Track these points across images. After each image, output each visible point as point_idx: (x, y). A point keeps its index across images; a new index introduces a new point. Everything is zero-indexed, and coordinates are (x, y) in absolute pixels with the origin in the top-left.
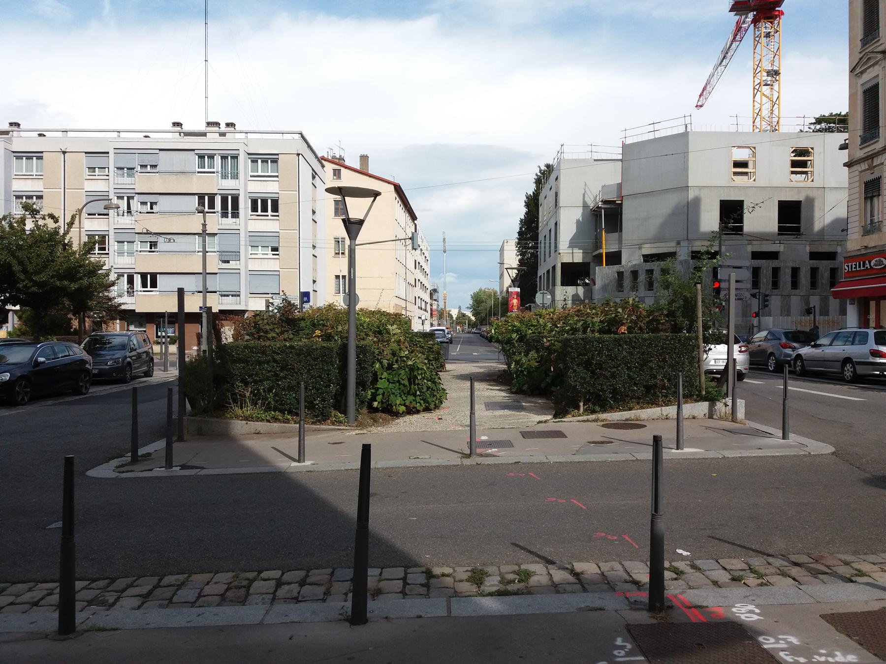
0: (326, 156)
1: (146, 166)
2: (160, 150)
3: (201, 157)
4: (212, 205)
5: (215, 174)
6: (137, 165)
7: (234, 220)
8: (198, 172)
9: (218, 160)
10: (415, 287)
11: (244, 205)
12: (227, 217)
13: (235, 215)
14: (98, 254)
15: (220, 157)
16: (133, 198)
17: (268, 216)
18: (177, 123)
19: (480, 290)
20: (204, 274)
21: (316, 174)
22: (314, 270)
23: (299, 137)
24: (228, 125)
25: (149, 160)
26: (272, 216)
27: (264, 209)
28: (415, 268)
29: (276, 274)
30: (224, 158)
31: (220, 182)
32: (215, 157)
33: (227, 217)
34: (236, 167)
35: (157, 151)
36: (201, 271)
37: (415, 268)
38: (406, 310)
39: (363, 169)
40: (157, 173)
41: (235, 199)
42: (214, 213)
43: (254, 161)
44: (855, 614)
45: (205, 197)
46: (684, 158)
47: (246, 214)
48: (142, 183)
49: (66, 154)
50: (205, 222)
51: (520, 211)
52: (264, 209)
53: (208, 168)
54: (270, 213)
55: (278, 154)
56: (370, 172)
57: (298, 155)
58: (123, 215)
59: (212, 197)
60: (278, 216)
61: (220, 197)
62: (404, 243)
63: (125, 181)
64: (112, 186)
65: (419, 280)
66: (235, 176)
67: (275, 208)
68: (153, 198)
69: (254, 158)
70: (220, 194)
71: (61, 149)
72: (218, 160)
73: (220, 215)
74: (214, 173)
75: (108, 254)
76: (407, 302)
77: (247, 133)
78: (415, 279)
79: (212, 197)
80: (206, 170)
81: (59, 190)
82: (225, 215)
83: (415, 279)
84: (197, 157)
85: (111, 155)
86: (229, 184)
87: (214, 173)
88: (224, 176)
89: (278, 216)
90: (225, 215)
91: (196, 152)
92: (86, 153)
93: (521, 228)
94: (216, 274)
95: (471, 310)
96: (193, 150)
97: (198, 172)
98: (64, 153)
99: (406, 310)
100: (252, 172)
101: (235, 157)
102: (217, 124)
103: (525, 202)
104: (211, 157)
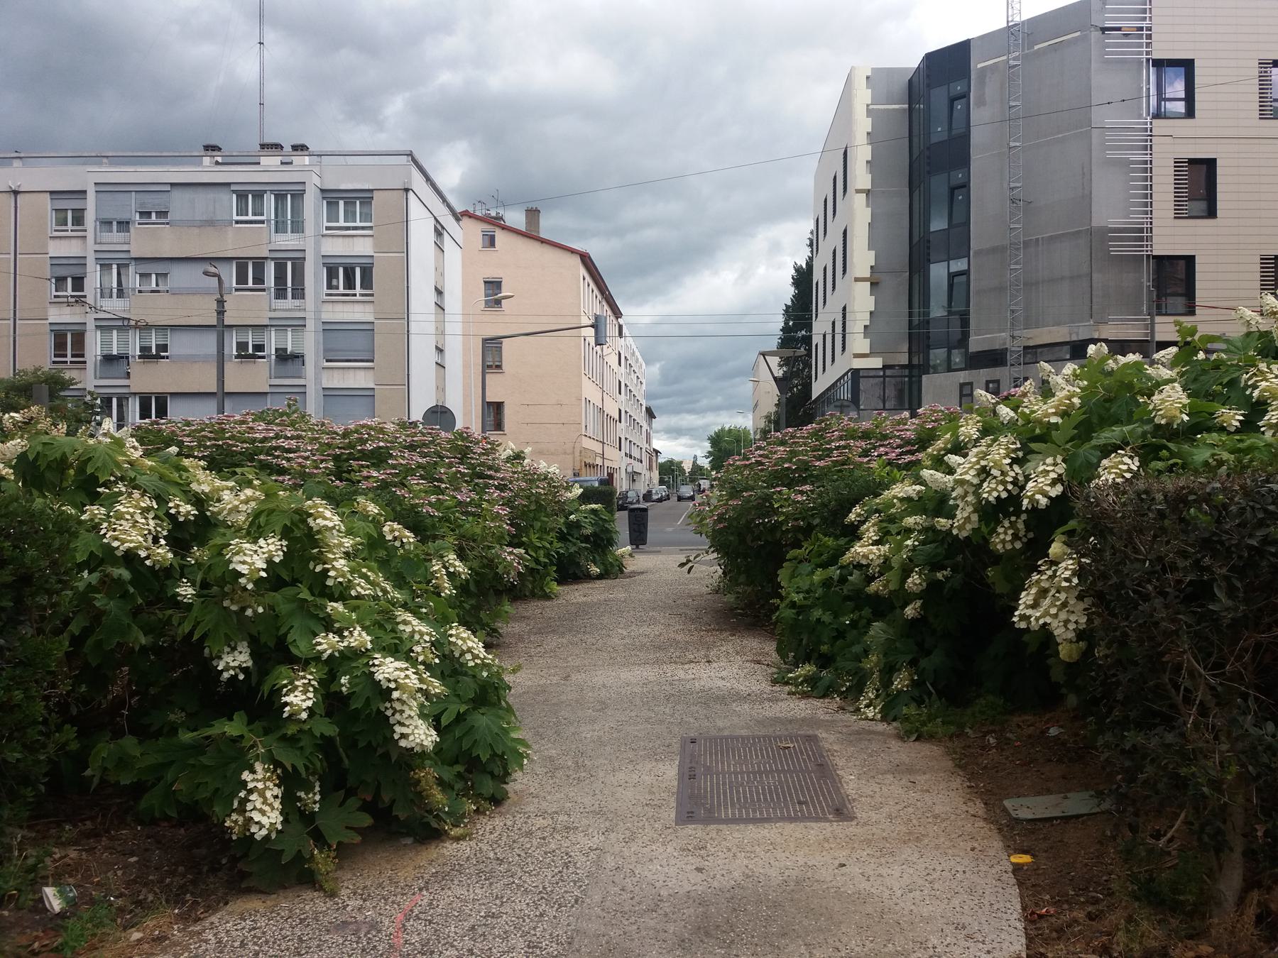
0: (471, 210)
1: (149, 214)
2: (172, 184)
3: (242, 196)
4: (259, 279)
5: (265, 225)
6: (133, 212)
7: (297, 302)
8: (237, 222)
9: (270, 202)
10: (620, 422)
11: (314, 277)
12: (285, 298)
13: (299, 293)
14: (71, 362)
15: (273, 196)
16: (127, 266)
17: (355, 295)
18: (212, 147)
19: (723, 429)
20: (220, 395)
21: (443, 228)
22: (440, 389)
23: (408, 161)
24: (296, 148)
25: (152, 203)
26: (362, 295)
27: (350, 284)
28: (620, 393)
29: (367, 395)
30: (280, 197)
31: (273, 239)
32: (265, 195)
33: (285, 298)
34: (297, 211)
35: (168, 188)
36: (214, 390)
37: (620, 393)
38: (603, 458)
39: (531, 231)
40: (168, 224)
41: (299, 265)
42: (264, 290)
43: (332, 204)
44: (463, 296)
45: (247, 263)
46: (1083, 178)
47: (317, 293)
48: (142, 241)
49: (18, 196)
50: (222, 296)
51: (787, 292)
52: (350, 284)
53: (254, 214)
54: (358, 290)
55: (372, 191)
56: (542, 235)
57: (407, 190)
58: (111, 297)
59: (259, 264)
60: (372, 295)
61: (273, 264)
62: (599, 352)
63: (114, 238)
64: (91, 245)
65: (626, 412)
66: (298, 227)
67: (367, 283)
68: (161, 268)
69: (331, 197)
70: (272, 259)
71: (11, 187)
72: (270, 202)
73: (273, 294)
74: (262, 222)
75: (85, 362)
76: (605, 445)
77: (321, 155)
78: (620, 411)
79: (259, 264)
80: (250, 217)
81: (7, 256)
82: (280, 293)
83: (620, 411)
84: (234, 196)
85: (91, 196)
86: (287, 241)
87: (262, 222)
88: (280, 228)
89: (372, 295)
90: (280, 293)
91: (233, 188)
92: (52, 192)
93: (786, 323)
94: (266, 393)
95: (709, 459)
96: (229, 184)
97: (237, 222)
98: (16, 193)
99: (603, 458)
100: (328, 221)
101: (298, 196)
102: (278, 146)
103: (793, 278)
104: (259, 196)
